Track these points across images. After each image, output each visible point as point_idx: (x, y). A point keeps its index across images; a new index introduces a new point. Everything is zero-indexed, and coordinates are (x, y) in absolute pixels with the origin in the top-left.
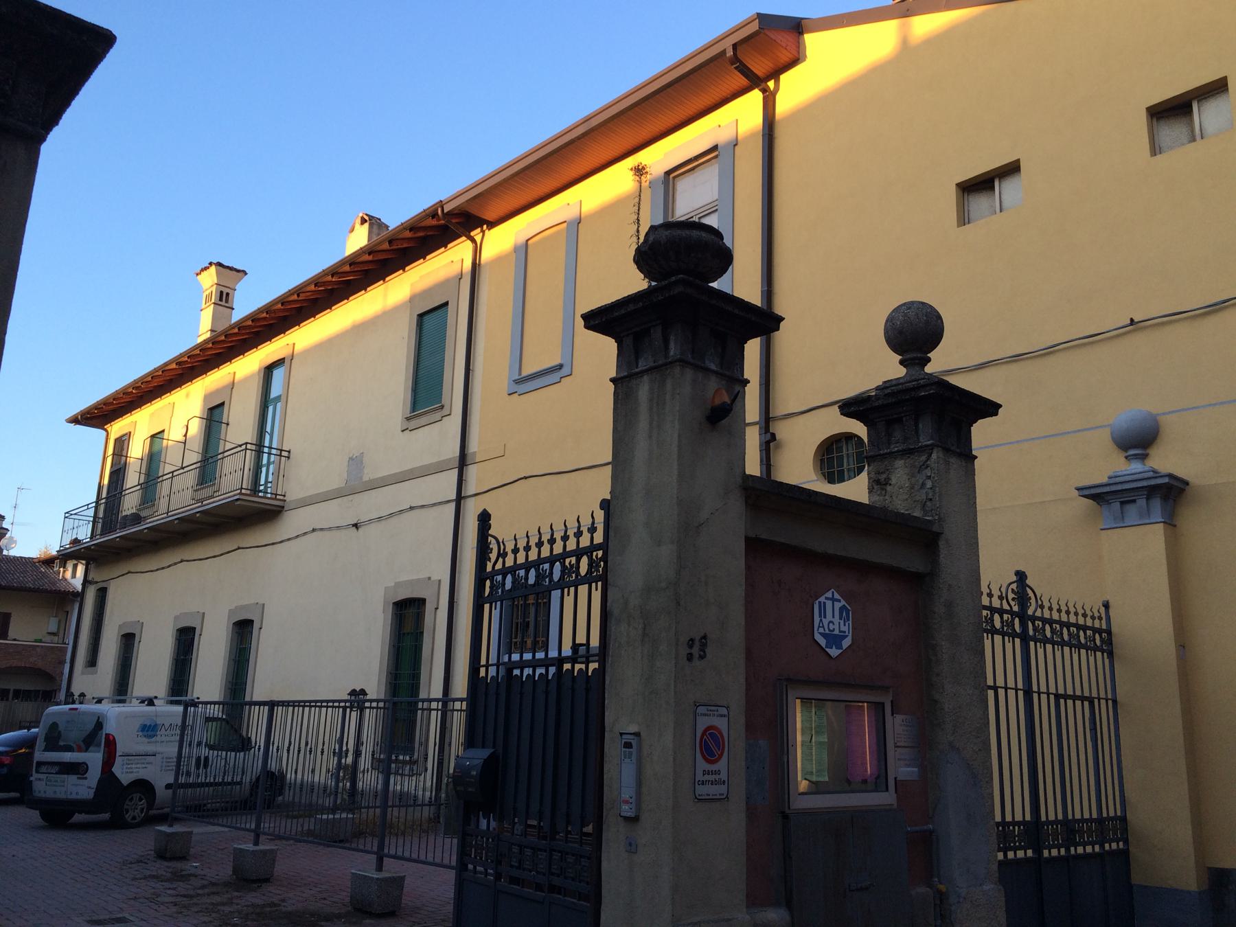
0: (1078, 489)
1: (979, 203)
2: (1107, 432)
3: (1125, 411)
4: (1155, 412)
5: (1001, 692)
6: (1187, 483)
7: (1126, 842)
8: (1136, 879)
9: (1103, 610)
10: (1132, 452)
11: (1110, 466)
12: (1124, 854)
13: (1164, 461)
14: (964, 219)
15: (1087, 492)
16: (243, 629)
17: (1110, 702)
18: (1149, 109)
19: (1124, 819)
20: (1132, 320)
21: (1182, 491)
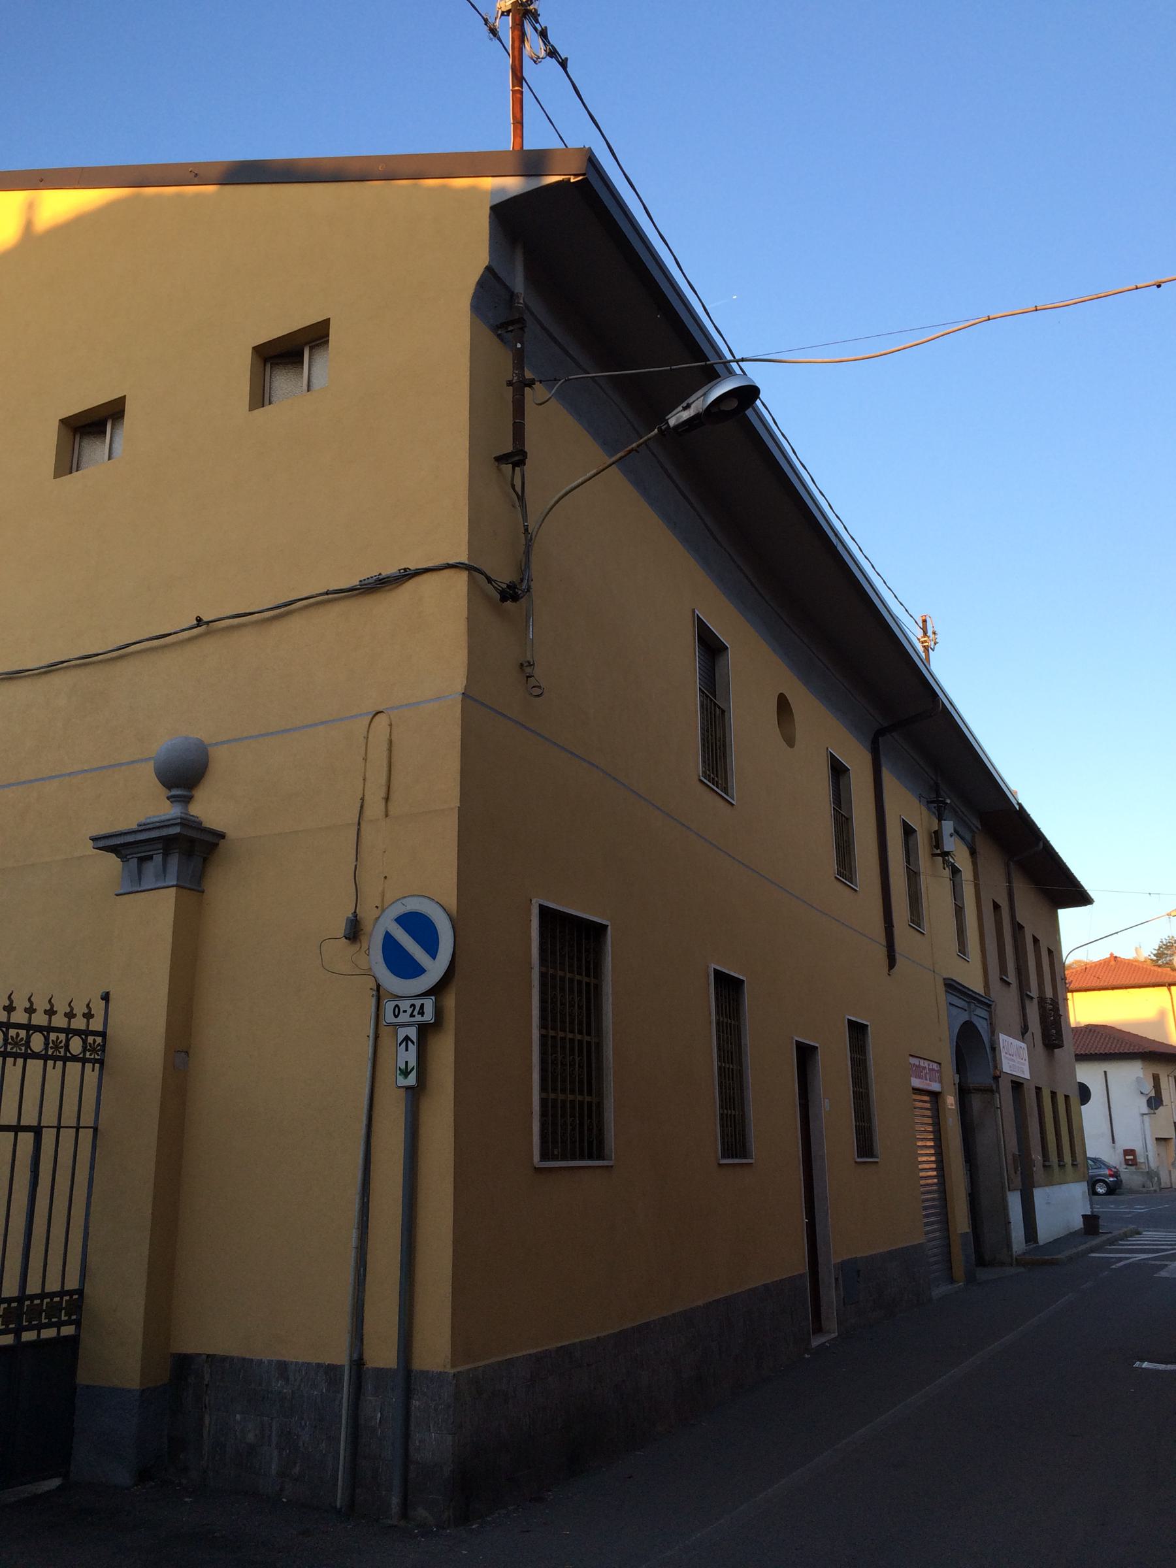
0: (94, 839)
1: (283, 382)
2: (151, 764)
3: (165, 737)
4: (207, 740)
5: (48, 1137)
6: (222, 836)
7: (78, 1323)
8: (83, 1377)
9: (98, 1007)
10: (175, 792)
11: (151, 806)
12: (74, 1340)
13: (209, 808)
14: (260, 397)
15: (101, 844)
16: (857, 1031)
17: (86, 1136)
18: (257, 350)
19: (80, 1292)
20: (199, 620)
21: (215, 846)
